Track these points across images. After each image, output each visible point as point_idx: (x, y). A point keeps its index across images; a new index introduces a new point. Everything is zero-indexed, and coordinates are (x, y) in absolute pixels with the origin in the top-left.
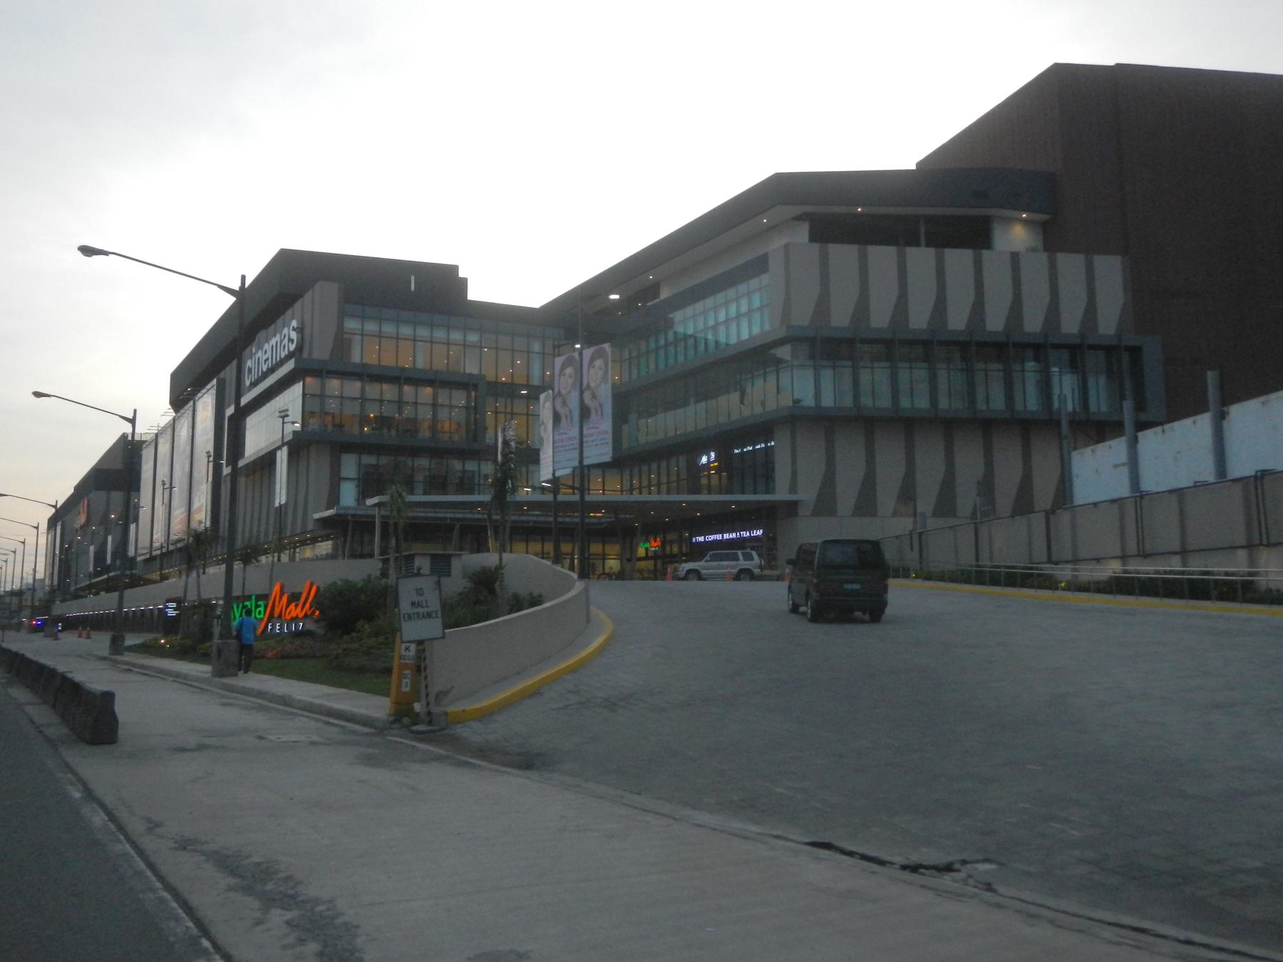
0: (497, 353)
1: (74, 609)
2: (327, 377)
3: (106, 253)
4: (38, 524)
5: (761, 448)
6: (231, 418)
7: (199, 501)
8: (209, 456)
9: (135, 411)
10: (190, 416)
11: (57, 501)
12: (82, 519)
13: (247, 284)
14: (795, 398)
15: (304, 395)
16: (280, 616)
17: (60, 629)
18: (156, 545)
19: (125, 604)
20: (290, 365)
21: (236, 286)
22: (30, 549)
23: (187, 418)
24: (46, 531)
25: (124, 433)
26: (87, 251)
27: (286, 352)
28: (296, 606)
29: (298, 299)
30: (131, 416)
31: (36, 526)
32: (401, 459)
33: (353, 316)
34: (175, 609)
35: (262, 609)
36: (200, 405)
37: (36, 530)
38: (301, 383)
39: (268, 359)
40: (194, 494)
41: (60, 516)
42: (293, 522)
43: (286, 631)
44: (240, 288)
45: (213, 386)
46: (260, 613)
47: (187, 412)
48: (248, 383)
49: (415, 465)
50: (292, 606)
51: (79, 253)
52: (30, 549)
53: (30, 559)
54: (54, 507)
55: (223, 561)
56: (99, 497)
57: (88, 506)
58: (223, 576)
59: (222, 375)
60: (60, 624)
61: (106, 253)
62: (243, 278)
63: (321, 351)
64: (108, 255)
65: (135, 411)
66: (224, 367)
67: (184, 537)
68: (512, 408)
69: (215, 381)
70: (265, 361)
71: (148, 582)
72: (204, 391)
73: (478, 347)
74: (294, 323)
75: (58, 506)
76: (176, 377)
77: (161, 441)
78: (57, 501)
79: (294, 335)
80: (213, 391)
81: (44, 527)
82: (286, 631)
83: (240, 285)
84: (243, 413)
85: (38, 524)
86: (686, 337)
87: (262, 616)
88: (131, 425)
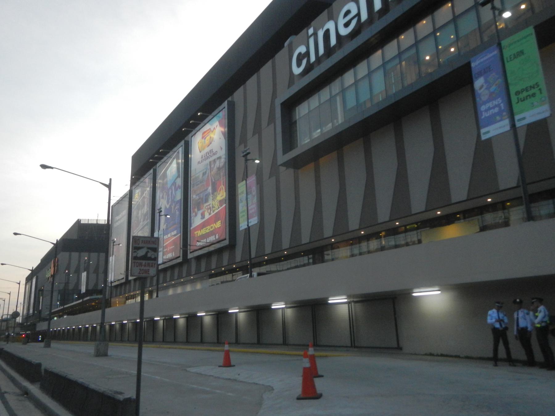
4: (20, 281)
9: (111, 180)
12: (51, 271)
21: (55, 242)
22: (7, 301)
23: (178, 158)
25: (78, 219)
30: (108, 183)
31: (19, 282)
44: (109, 184)
52: (7, 301)
56: (63, 256)
60: (40, 336)
61: (20, 234)
62: (33, 267)
65: (111, 180)
68: (190, 248)
69: (225, 104)
72: (210, 117)
76: (136, 158)
81: (23, 282)
83: (109, 182)
88: (108, 189)
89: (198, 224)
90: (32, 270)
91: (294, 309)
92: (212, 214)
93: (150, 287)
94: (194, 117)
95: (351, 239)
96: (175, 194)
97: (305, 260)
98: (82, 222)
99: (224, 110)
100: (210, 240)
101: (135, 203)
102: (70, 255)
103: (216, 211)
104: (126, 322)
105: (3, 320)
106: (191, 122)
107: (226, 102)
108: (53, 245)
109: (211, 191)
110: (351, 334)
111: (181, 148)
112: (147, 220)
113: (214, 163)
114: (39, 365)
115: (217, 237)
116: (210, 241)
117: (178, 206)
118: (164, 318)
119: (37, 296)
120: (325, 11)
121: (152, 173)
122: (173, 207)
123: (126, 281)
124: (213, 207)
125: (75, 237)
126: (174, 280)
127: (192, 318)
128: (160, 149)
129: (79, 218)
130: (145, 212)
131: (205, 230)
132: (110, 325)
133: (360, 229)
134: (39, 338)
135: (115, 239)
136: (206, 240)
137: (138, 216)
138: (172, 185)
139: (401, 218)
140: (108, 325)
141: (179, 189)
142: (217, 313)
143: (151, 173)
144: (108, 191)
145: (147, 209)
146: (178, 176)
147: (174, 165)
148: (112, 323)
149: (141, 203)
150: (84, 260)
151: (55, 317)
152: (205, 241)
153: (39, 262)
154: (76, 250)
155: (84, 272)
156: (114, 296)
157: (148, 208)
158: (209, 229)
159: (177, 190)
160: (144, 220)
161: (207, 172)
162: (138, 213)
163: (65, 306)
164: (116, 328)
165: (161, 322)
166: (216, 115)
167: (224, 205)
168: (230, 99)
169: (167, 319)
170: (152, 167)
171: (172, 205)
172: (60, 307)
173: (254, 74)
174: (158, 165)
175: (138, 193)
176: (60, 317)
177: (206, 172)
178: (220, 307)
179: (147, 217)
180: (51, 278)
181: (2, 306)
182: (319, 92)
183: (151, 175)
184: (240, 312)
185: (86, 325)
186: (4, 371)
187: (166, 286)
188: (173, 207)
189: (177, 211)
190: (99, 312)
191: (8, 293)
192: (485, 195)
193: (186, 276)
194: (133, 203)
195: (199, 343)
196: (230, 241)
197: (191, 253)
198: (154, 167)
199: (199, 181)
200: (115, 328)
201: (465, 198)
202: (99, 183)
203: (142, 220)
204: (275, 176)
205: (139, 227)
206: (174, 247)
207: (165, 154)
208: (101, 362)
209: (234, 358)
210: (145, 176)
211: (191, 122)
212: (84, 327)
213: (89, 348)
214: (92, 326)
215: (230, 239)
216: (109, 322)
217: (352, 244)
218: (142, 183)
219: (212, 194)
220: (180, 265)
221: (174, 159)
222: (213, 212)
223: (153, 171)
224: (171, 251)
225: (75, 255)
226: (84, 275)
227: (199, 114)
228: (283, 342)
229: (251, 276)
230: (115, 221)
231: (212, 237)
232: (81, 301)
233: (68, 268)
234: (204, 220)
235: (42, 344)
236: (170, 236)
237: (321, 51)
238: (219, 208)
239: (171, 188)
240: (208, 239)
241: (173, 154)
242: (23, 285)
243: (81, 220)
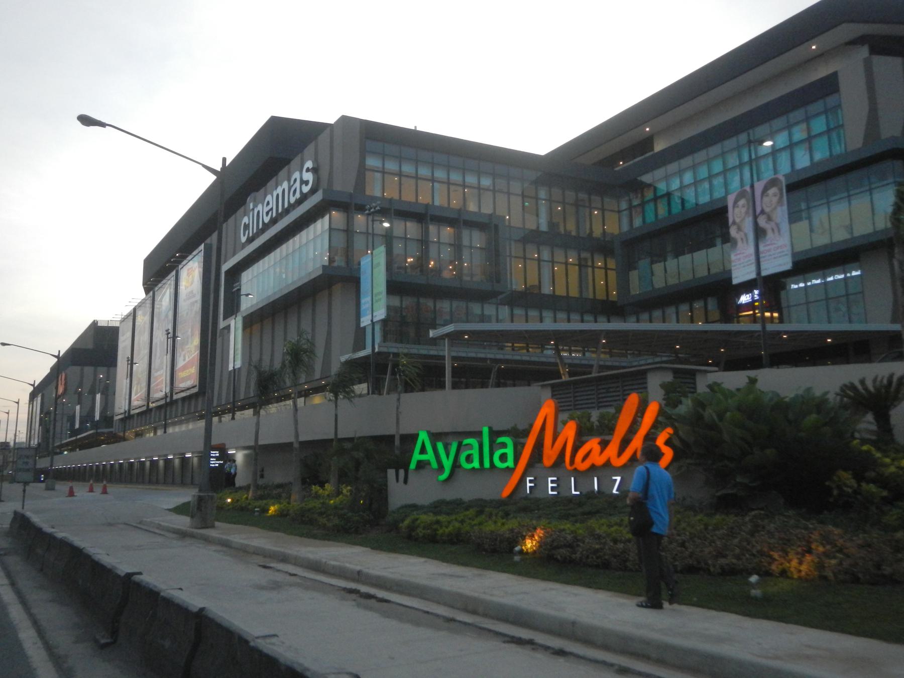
0: (509, 198)
1: (67, 460)
2: (355, 213)
3: (103, 125)
4: (19, 400)
5: (799, 288)
6: (227, 272)
7: (184, 360)
8: (168, 334)
10: (173, 287)
11: (35, 381)
13: (227, 164)
14: (795, 251)
15: (331, 229)
16: (559, 462)
17: (42, 479)
18: (135, 403)
19: (54, 465)
20: (317, 198)
21: (218, 167)
22: (13, 416)
24: (28, 402)
25: (95, 321)
26: (86, 120)
27: (298, 195)
28: (604, 444)
29: (281, 168)
31: (17, 401)
32: (422, 300)
33: (374, 153)
34: (218, 459)
35: (509, 451)
36: (184, 274)
37: (17, 405)
38: (328, 215)
39: (272, 209)
40: (177, 354)
41: (38, 391)
42: (218, 397)
43: (615, 491)
45: (173, 276)
46: (503, 458)
47: (169, 282)
48: (244, 239)
49: (437, 308)
50: (593, 444)
51: (79, 123)
52: (13, 416)
53: (12, 428)
54: (33, 385)
55: (201, 417)
57: (66, 379)
58: (203, 431)
59: (208, 241)
60: (43, 476)
61: (103, 125)
62: (224, 160)
63: (343, 185)
64: (105, 127)
66: (210, 235)
67: (195, 384)
69: (202, 247)
70: (267, 213)
71: (124, 439)
72: (190, 257)
73: (490, 190)
74: (309, 164)
75: (36, 385)
76: (149, 262)
77: (139, 313)
78: (35, 381)
79: (308, 176)
80: (202, 253)
82: (615, 491)
83: (221, 166)
84: (235, 273)
85: (19, 400)
86: (668, 195)
87: (510, 463)
89: (181, 365)
92: (191, 358)
98: (99, 325)
99: (200, 254)
101: (139, 324)
102: (82, 371)
103: (193, 356)
107: (203, 245)
108: (212, 178)
115: (192, 383)
119: (235, 307)
120: (261, 190)
123: (199, 390)
125: (90, 346)
128: (166, 263)
129: (95, 319)
132: (165, 459)
133: (321, 379)
134: (41, 478)
140: (162, 459)
146: (170, 310)
148: (142, 460)
151: (66, 450)
153: (48, 371)
154: (91, 364)
155: (98, 394)
156: (179, 415)
163: (79, 437)
164: (193, 463)
165: (195, 460)
166: (191, 259)
167: (197, 352)
170: (204, 242)
173: (271, 179)
174: (180, 266)
176: (70, 451)
181: (4, 426)
182: (315, 224)
185: (153, 457)
196: (199, 388)
197: (176, 394)
198: (177, 269)
200: (191, 464)
209: (109, 490)
212: (137, 462)
214: (151, 461)
219: (191, 337)
221: (167, 288)
223: (176, 272)
225: (89, 370)
226: (98, 396)
227: (177, 255)
229: (233, 418)
232: (74, 438)
233: (81, 385)
234: (185, 362)
235: (43, 485)
237: (255, 231)
243: (97, 322)
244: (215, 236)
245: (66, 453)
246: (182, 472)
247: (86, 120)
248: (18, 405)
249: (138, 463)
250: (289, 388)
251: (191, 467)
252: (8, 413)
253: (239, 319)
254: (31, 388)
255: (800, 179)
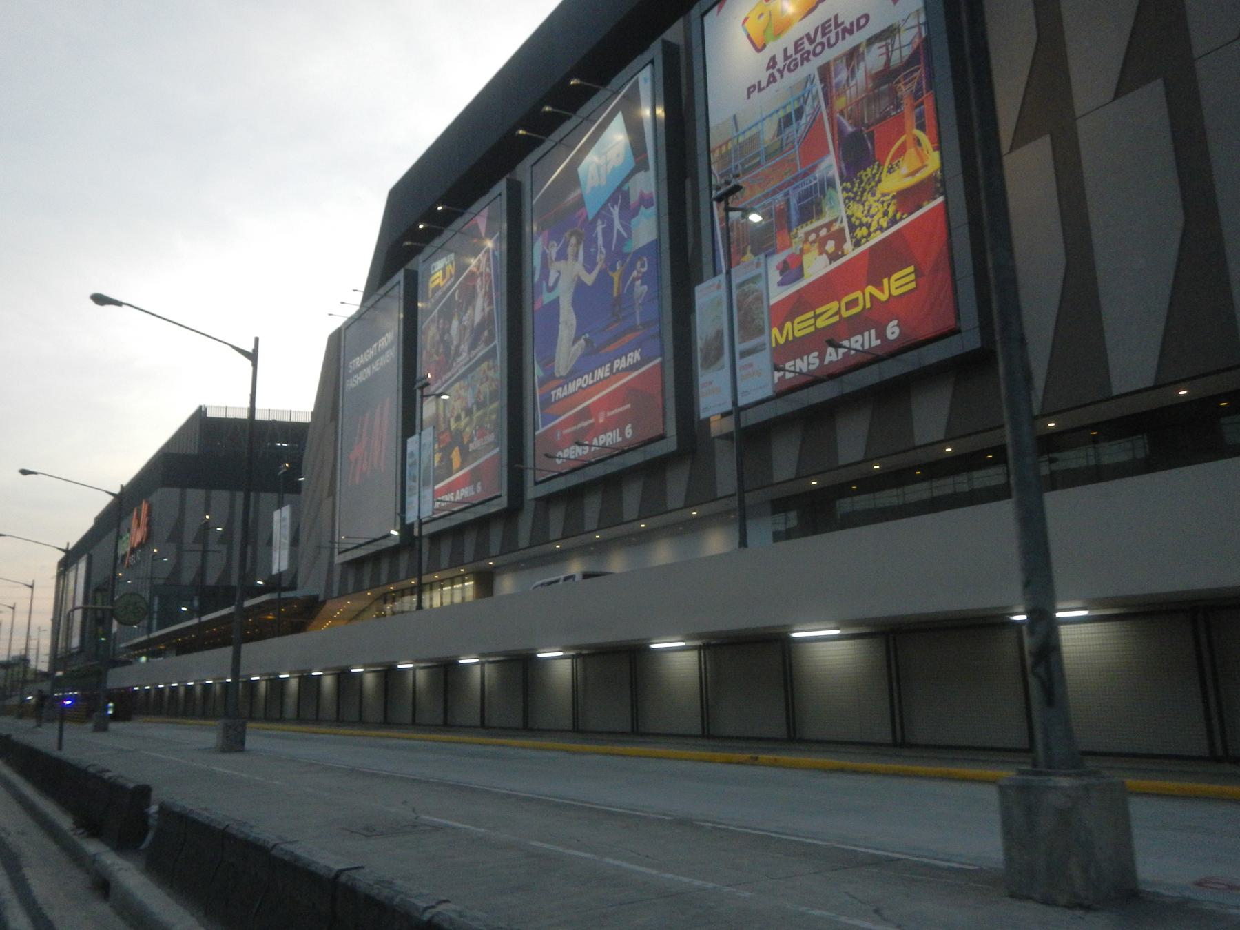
3: (118, 304)
9: (257, 340)
25: (201, 407)
26: (100, 299)
30: (250, 349)
51: (92, 303)
56: (166, 497)
57: (149, 513)
60: (111, 705)
61: (118, 304)
62: (68, 544)
65: (257, 340)
90: (66, 551)
91: (858, 641)
93: (389, 583)
94: (412, 232)
95: (1093, 427)
96: (627, 228)
97: (1115, 452)
98: (210, 414)
100: (462, 494)
103: (878, 237)
104: (258, 678)
105: (6, 665)
106: (572, 83)
108: (110, 498)
109: (834, 172)
110: (702, 708)
111: (648, 68)
112: (488, 342)
113: (848, 66)
114: (143, 792)
116: (463, 497)
117: (643, 266)
118: (266, 678)
121: (402, 283)
122: (616, 277)
124: (852, 228)
125: (193, 449)
126: (440, 570)
127: (389, 675)
129: (202, 404)
130: (477, 319)
131: (812, 321)
133: (868, 460)
135: (429, 375)
136: (454, 496)
137: (446, 338)
138: (608, 201)
139: (1059, 412)
141: (647, 207)
142: (385, 668)
143: (399, 283)
144: (251, 369)
145: (487, 309)
147: (616, 136)
148: (208, 682)
149: (457, 298)
150: (151, 555)
152: (452, 499)
157: (490, 303)
158: (838, 312)
159: (635, 213)
160: (473, 346)
161: (808, 110)
162: (445, 331)
163: (205, 618)
165: (263, 684)
168: (508, 176)
169: (586, 655)
171: (614, 270)
172: (157, 631)
175: (444, 269)
177: (799, 112)
178: (442, 653)
179: (486, 333)
180: (130, 555)
183: (398, 286)
184: (365, 672)
185: (205, 680)
186: (9, 786)
187: (561, 552)
188: (616, 277)
189: (638, 283)
190: (228, 651)
191: (28, 586)
192: (1176, 382)
193: (450, 567)
194: (420, 305)
195: (517, 729)
197: (340, 553)
198: (674, 33)
199: (758, 154)
201: (1150, 383)
202: (229, 347)
203: (465, 347)
204: (1048, 136)
205: (453, 371)
206: (628, 406)
207: (584, 95)
208: (226, 765)
210: (475, 208)
211: (572, 83)
213: (207, 735)
215: (509, 496)
216: (203, 681)
217: (1095, 440)
218: (458, 236)
220: (655, 469)
222: (857, 244)
224: (617, 423)
225: (195, 496)
228: (633, 728)
230: (350, 371)
231: (610, 434)
236: (607, 374)
238: (894, 221)
239: (604, 213)
240: (458, 492)
241: (609, 100)
242: (52, 578)
243: (206, 409)
244: (678, 26)
245: (143, 659)
246: (338, 704)
247: (100, 299)
248: (14, 612)
249: (268, 682)
250: (557, 541)
251: (410, 696)
252: (32, 587)
253: (847, 195)
254: (62, 554)
255: (551, 492)
